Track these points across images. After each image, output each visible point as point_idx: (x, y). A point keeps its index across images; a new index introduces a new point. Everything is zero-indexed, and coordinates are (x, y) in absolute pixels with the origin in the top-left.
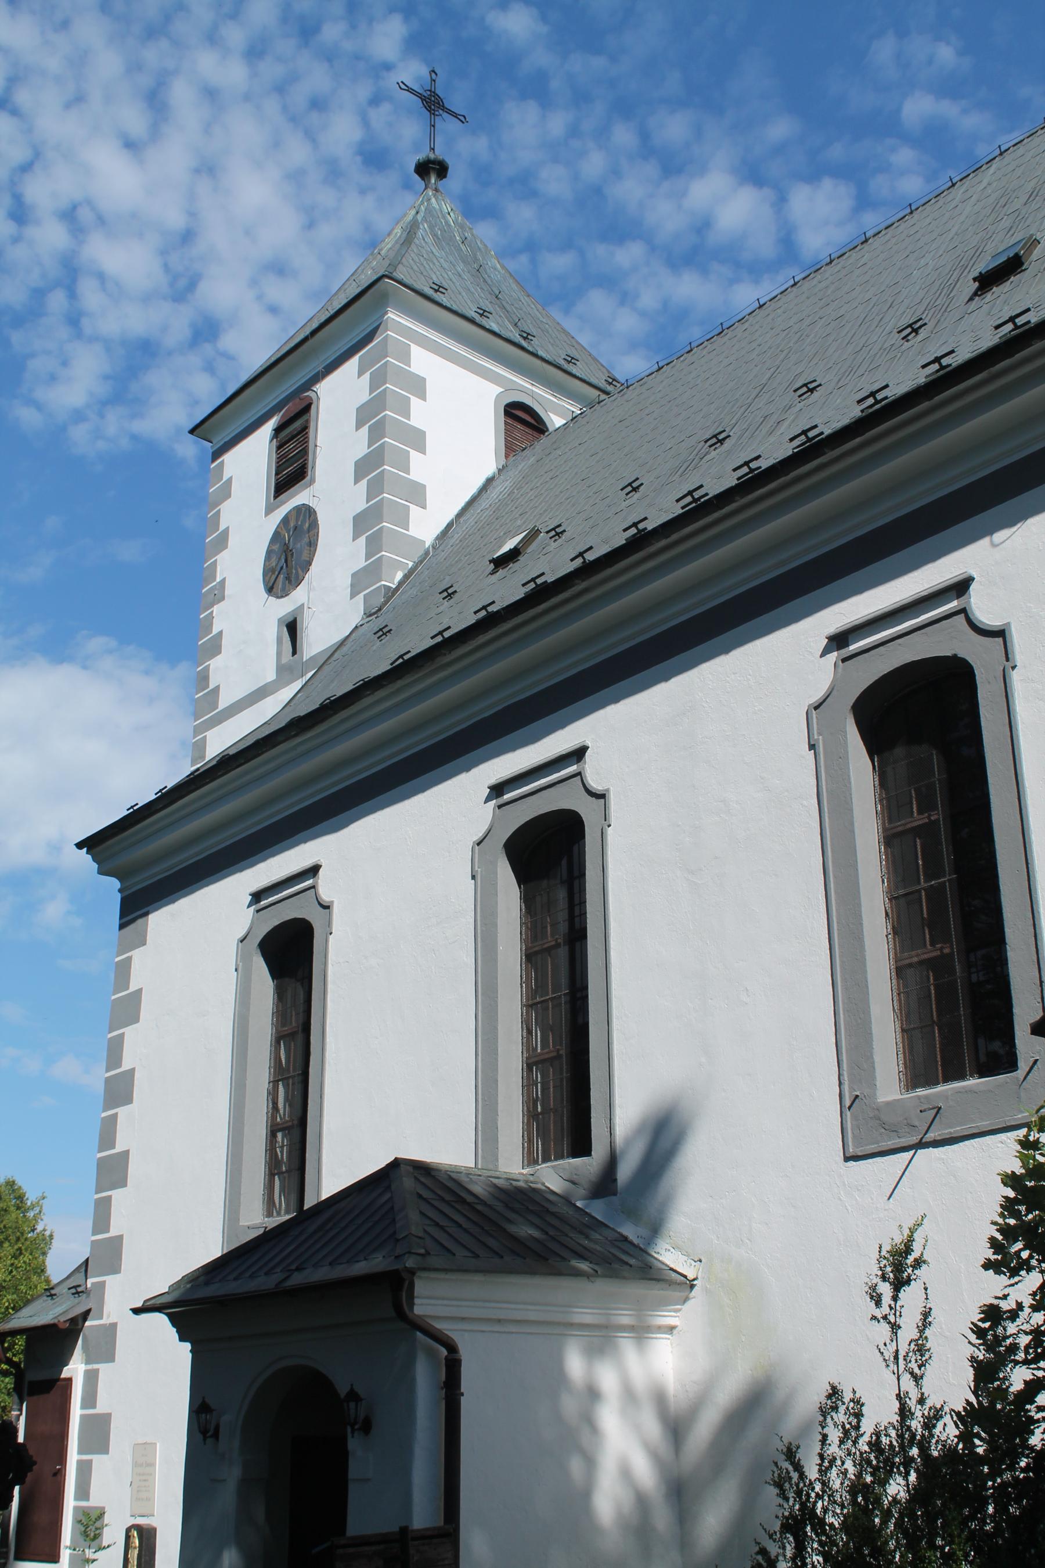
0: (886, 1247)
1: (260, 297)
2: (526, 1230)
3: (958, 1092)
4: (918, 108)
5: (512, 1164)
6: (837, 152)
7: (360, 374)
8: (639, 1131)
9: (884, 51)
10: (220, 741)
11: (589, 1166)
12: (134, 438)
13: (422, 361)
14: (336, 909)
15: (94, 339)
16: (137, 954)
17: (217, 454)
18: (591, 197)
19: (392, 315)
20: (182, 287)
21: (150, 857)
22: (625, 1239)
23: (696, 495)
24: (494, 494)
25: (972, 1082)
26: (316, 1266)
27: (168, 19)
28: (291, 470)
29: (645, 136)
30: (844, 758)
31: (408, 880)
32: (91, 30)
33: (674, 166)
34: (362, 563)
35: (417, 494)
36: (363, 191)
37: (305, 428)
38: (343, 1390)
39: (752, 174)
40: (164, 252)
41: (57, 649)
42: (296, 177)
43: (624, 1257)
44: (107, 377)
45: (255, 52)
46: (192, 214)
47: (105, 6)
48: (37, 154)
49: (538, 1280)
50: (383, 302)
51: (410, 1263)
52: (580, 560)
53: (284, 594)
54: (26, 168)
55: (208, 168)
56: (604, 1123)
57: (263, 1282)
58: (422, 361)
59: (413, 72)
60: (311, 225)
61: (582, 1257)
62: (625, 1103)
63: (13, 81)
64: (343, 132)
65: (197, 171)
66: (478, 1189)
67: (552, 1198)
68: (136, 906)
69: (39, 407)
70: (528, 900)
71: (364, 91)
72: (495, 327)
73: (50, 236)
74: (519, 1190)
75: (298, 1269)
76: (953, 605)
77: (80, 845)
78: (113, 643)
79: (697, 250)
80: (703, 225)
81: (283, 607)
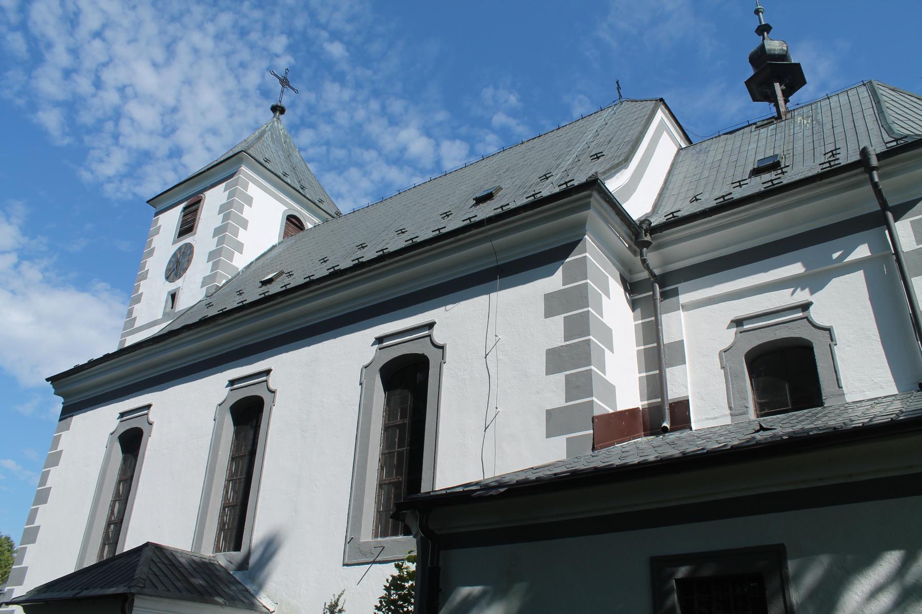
0: (328, 604)
1: (203, 142)
2: (198, 581)
3: (392, 541)
4: (499, 119)
5: (207, 552)
6: (463, 130)
8: (261, 543)
9: (488, 93)
10: (131, 341)
11: (238, 556)
12: (135, 194)
13: (253, 190)
14: (154, 426)
15: (122, 147)
16: (64, 434)
17: (157, 214)
18: (357, 129)
19: (243, 168)
20: (168, 131)
21: (79, 389)
22: (247, 590)
24: (274, 253)
25: (400, 537)
26: (94, 588)
27: (182, 15)
28: (187, 227)
29: (383, 107)
30: (372, 390)
31: (187, 416)
32: (146, 13)
33: (394, 122)
34: (209, 273)
35: (240, 247)
36: (257, 106)
37: (197, 210)
39: (427, 132)
40: (163, 115)
41: (82, 285)
42: (228, 94)
43: (242, 598)
44: (126, 165)
45: (219, 37)
46: (178, 101)
47: (154, 4)
48: (111, 60)
49: (197, 605)
50: (240, 162)
51: (133, 591)
54: (105, 65)
55: (188, 82)
56: (249, 537)
57: (69, 594)
58: (253, 190)
59: (284, 62)
60: (231, 116)
61: (222, 597)
62: (259, 529)
63: (105, 26)
64: (252, 79)
65: (184, 82)
66: (183, 560)
67: (218, 568)
68: (68, 412)
69: (92, 172)
70: (237, 433)
71: (264, 64)
72: (289, 181)
73: (111, 97)
74: (204, 563)
75: (86, 589)
76: (426, 332)
77: (48, 380)
78: (109, 287)
79: (399, 159)
80: (403, 149)
81: (171, 287)
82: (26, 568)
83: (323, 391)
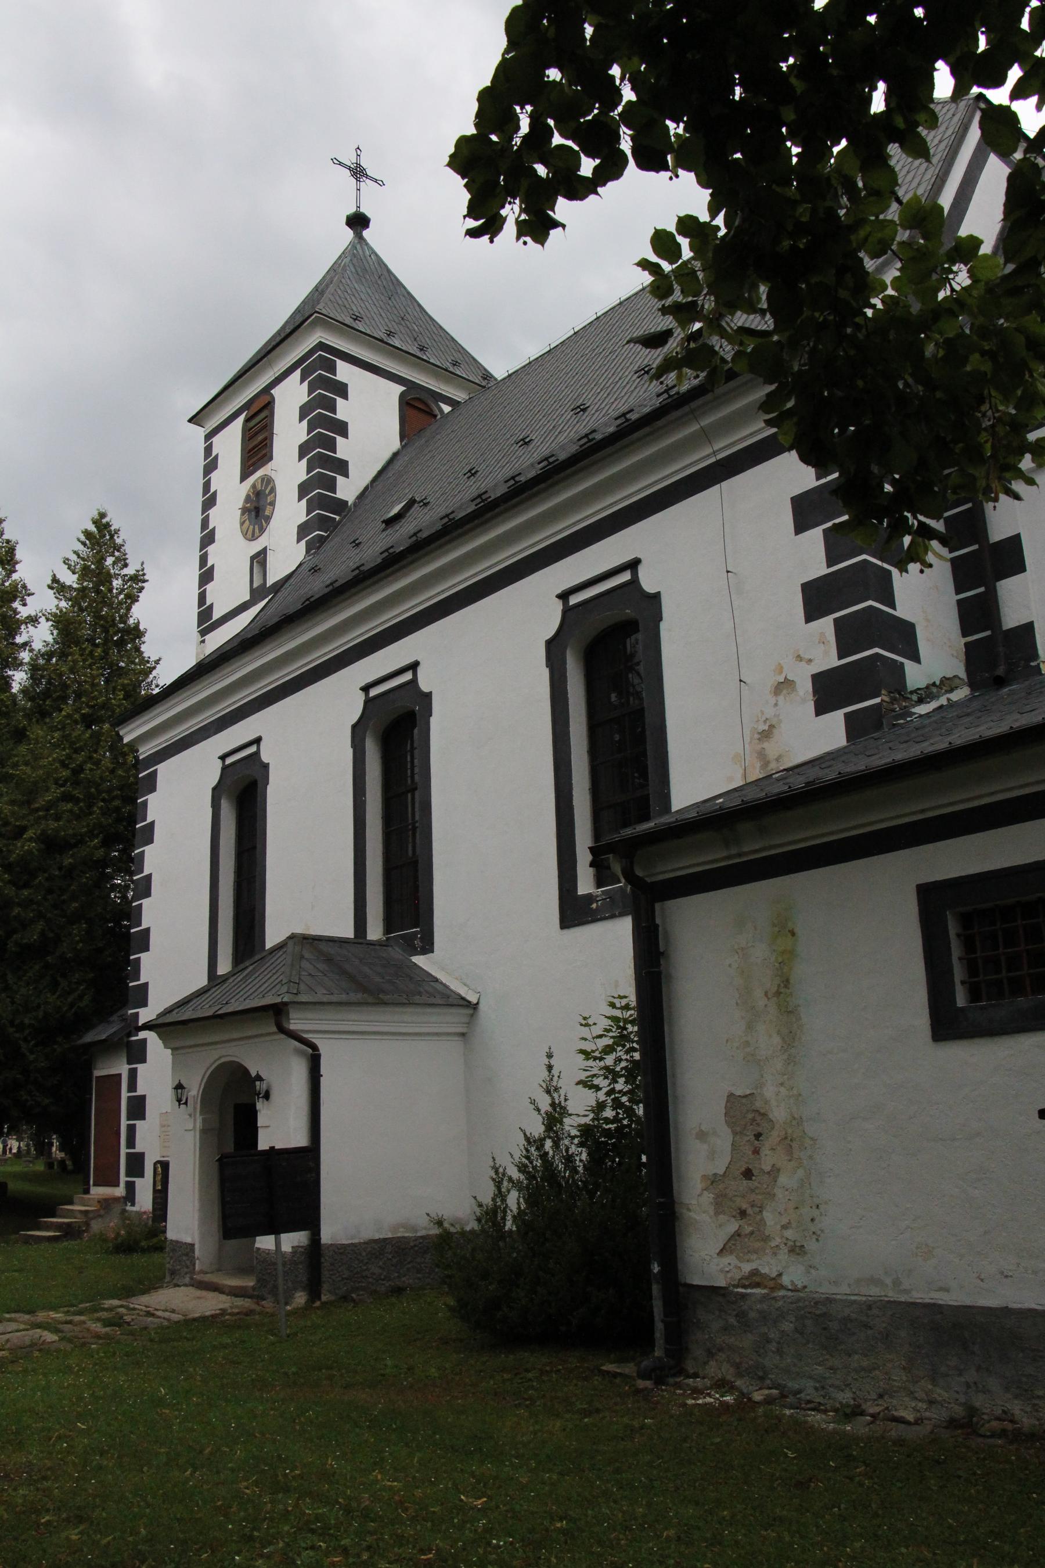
7: (302, 381)
23: (484, 497)
35: (342, 467)
38: (253, 1074)
52: (414, 538)
53: (253, 538)
72: (397, 344)
82: (153, 823)
83: (490, 675)
